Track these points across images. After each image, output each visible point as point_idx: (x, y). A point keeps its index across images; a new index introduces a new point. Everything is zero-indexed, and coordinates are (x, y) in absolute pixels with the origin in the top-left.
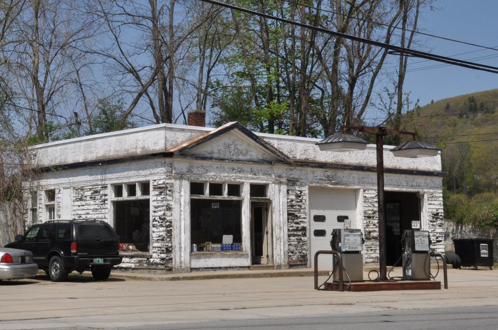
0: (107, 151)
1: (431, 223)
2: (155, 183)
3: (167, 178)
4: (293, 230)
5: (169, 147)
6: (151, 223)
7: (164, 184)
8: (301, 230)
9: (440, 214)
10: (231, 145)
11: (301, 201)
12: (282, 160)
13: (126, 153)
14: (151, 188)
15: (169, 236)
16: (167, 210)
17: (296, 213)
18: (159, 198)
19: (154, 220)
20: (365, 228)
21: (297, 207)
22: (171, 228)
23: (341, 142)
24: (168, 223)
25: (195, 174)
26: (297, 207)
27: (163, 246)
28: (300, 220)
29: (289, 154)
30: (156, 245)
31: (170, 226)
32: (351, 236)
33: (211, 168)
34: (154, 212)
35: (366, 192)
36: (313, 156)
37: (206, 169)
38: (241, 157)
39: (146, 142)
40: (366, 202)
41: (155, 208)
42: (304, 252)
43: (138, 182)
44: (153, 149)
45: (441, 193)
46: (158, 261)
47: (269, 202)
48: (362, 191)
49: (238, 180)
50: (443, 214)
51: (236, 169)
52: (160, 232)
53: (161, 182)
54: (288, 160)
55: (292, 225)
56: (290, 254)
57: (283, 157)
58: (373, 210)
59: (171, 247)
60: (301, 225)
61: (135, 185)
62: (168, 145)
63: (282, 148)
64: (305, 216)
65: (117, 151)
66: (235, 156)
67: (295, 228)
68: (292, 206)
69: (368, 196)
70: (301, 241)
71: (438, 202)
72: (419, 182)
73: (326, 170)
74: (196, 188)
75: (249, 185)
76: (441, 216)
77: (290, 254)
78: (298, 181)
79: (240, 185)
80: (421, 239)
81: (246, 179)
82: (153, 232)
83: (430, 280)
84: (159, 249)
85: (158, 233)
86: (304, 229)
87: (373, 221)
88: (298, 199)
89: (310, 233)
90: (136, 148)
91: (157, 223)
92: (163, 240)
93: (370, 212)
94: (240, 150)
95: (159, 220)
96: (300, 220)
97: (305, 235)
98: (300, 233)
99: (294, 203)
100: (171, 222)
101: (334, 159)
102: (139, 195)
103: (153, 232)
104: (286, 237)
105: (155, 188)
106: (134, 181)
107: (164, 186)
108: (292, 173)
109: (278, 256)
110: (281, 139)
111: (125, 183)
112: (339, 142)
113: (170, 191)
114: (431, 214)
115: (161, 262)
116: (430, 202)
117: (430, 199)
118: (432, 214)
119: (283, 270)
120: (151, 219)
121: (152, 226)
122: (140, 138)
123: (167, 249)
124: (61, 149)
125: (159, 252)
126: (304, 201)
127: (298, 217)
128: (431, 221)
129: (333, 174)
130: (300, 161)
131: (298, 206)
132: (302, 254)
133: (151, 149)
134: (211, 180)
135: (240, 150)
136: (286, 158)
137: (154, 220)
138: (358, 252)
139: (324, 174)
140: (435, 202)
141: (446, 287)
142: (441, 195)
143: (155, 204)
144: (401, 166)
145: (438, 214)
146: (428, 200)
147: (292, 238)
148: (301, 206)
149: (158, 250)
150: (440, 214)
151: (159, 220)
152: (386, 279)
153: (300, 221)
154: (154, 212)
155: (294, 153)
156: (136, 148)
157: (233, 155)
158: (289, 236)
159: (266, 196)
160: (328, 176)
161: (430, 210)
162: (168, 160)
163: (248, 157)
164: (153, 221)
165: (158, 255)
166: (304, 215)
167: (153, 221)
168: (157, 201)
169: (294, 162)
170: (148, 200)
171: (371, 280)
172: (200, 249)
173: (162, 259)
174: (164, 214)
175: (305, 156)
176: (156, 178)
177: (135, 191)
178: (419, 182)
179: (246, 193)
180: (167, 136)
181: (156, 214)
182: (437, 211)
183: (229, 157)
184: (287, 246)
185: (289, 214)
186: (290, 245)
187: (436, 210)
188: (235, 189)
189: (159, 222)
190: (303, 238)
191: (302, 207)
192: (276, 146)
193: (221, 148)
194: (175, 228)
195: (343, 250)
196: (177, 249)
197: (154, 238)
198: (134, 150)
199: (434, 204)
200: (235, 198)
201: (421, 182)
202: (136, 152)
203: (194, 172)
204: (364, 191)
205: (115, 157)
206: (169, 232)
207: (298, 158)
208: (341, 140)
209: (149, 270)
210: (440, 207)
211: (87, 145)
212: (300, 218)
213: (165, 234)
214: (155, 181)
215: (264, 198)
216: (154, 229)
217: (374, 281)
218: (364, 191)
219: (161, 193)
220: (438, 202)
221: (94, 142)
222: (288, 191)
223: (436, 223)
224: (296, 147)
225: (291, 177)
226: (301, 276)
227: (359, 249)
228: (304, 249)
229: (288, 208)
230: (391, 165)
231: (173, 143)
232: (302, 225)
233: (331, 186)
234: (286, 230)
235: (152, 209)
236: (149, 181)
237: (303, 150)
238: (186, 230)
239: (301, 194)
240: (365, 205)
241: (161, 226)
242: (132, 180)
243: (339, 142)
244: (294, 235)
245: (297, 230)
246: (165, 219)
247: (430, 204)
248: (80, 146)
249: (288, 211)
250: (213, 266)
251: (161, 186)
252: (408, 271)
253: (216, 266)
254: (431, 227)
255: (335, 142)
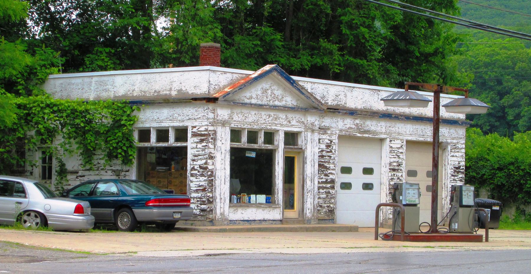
0: (129, 91)
1: (453, 177)
2: (195, 130)
3: (210, 125)
4: (322, 182)
5: (212, 92)
6: (188, 172)
7: (206, 130)
8: (330, 183)
9: (462, 168)
10: (268, 90)
11: (331, 151)
12: (316, 106)
13: (156, 94)
14: (189, 135)
15: (210, 186)
16: (209, 159)
17: (326, 165)
18: (200, 146)
19: (193, 169)
20: (389, 181)
21: (327, 157)
22: (212, 178)
23: (408, 99)
24: (209, 173)
25: (235, 121)
26: (327, 157)
27: (204, 197)
28: (329, 171)
29: (321, 100)
30: (194, 195)
31: (211, 175)
32: (410, 190)
33: (250, 115)
34: (194, 160)
35: (393, 142)
36: (344, 102)
37: (245, 115)
38: (277, 103)
39: (183, 84)
40: (392, 153)
41: (194, 156)
42: (332, 206)
43: (173, 127)
44: (192, 93)
45: (464, 144)
46: (197, 212)
47: (301, 151)
48: (388, 140)
49: (273, 127)
50: (464, 167)
51: (273, 115)
52: (200, 181)
53: (203, 129)
54: (321, 106)
55: (321, 177)
56: (319, 208)
57: (317, 103)
58: (398, 162)
59: (212, 197)
60: (330, 177)
61: (169, 130)
62: (211, 89)
63: (315, 93)
64: (334, 168)
65: (144, 92)
66: (271, 101)
67: (324, 180)
68: (322, 156)
69: (393, 146)
70: (329, 195)
71: (460, 154)
72: (444, 132)
73: (355, 117)
74: (235, 134)
75: (283, 133)
76: (462, 169)
77: (319, 208)
78: (329, 129)
79: (241, 131)
80: (467, 194)
81: (281, 127)
82: (192, 182)
83: (473, 233)
84: (199, 200)
85: (198, 183)
86: (333, 181)
87: (398, 174)
88: (328, 149)
89: (337, 186)
90: (171, 90)
91: (197, 172)
92: (204, 190)
93: (395, 164)
94: (276, 95)
95: (198, 169)
96: (329, 171)
97: (333, 188)
98: (329, 185)
99: (324, 153)
100: (212, 172)
101: (364, 105)
102: (172, 141)
103: (192, 182)
104: (316, 189)
105: (195, 135)
106: (167, 126)
107: (206, 133)
108: (323, 120)
109: (309, 209)
110: (314, 83)
111: (153, 128)
112: (405, 100)
113: (212, 139)
114: (453, 168)
115: (201, 213)
116: (452, 154)
117: (453, 151)
118: (454, 167)
119: (313, 225)
120: (189, 168)
121: (190, 175)
122: (175, 79)
123: (208, 200)
124: (62, 84)
125: (199, 203)
126: (333, 151)
127: (327, 168)
128: (452, 176)
129: (361, 122)
130: (332, 107)
131: (328, 156)
132: (330, 209)
133: (190, 92)
134: (249, 127)
135: (276, 95)
136: (320, 104)
137: (193, 169)
138: (415, 205)
139: (354, 122)
140: (457, 154)
141: (487, 240)
142: (464, 146)
143: (194, 151)
144: (427, 114)
145: (459, 168)
146: (451, 151)
147: (321, 191)
148: (330, 157)
149: (198, 201)
150: (462, 168)
151: (198, 169)
152: (437, 231)
153: (329, 173)
154: (194, 160)
155: (326, 99)
156: (171, 90)
157: (270, 100)
158: (319, 188)
159: (297, 145)
160: (357, 124)
161: (453, 163)
162: (211, 106)
163: (283, 103)
164: (191, 170)
165: (198, 206)
166: (333, 166)
167: (191, 170)
168: (196, 148)
169: (328, 109)
170: (186, 148)
171: (422, 233)
172: (239, 200)
173: (203, 210)
174: (206, 163)
175: (336, 102)
176: (196, 124)
177: (168, 137)
178: (444, 132)
179: (280, 140)
180: (211, 79)
181: (195, 163)
182: (459, 164)
183: (266, 103)
184: (316, 199)
185: (320, 165)
186: (319, 198)
187: (457, 163)
188: (270, 137)
189: (199, 172)
190: (331, 191)
191: (332, 158)
192: (309, 91)
193: (259, 92)
194: (217, 178)
195: (404, 203)
196: (218, 200)
197: (191, 188)
198: (168, 93)
199: (456, 156)
200: (270, 147)
201: (445, 131)
202: (170, 95)
203: (234, 119)
204: (391, 141)
205: (141, 98)
206: (211, 183)
207: (330, 104)
208: (408, 98)
209: (185, 222)
210: (463, 160)
211: (101, 82)
212: (329, 170)
213: (206, 184)
214: (195, 127)
215: (296, 147)
216: (192, 179)
217: (425, 233)
218: (391, 141)
219: (202, 141)
220: (460, 154)
221: (113, 77)
222: (319, 139)
223: (457, 178)
224: (329, 92)
225: (323, 125)
226: (333, 231)
227: (417, 202)
228: (332, 203)
229: (319, 159)
230: (418, 112)
231: (216, 87)
232: (331, 176)
233: (359, 135)
234: (316, 183)
235: (190, 157)
236: (187, 127)
237: (334, 96)
238: (226, 180)
239: (331, 143)
240: (391, 156)
241: (202, 175)
242: (165, 124)
243: (405, 100)
244: (323, 188)
245: (326, 182)
246: (207, 168)
247: (453, 156)
248: (91, 82)
249: (319, 161)
250: (249, 219)
251: (203, 133)
252: (454, 224)
253: (251, 219)
254: (452, 181)
255: (402, 99)
